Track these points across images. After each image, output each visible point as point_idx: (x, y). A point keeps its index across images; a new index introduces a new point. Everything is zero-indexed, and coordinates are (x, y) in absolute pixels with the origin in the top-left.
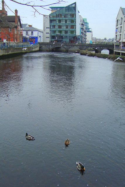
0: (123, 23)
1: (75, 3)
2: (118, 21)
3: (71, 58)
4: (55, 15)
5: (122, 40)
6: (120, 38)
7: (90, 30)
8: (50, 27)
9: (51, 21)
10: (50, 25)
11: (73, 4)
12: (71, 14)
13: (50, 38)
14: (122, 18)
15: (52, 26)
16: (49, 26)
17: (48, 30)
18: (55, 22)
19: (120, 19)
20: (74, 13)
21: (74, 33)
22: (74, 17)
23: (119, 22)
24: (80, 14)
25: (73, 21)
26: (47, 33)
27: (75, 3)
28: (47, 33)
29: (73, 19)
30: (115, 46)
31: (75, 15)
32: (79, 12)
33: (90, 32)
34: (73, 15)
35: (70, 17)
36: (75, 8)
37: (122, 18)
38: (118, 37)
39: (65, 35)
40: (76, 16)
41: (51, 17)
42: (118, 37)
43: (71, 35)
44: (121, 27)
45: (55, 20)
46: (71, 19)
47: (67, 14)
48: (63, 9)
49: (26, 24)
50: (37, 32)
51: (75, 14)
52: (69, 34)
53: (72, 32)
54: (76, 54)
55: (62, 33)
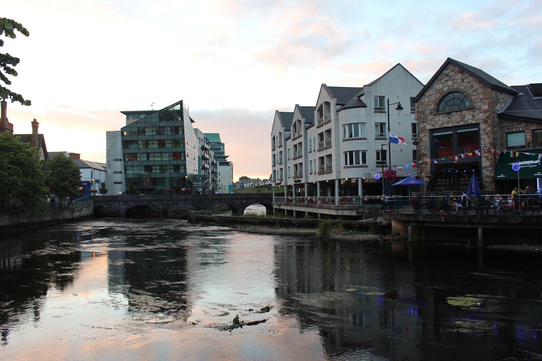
0: (283, 143)
1: (181, 103)
2: (274, 139)
3: (77, 265)
4: (136, 130)
5: (307, 177)
6: (281, 176)
7: (228, 160)
8: (124, 158)
9: (126, 144)
10: (124, 154)
11: (177, 104)
12: (171, 127)
13: (124, 183)
14: (280, 133)
15: (127, 156)
16: (120, 156)
17: (119, 166)
18: (134, 146)
19: (277, 135)
20: (180, 124)
21: (182, 171)
22: (180, 133)
23: (277, 143)
24: (194, 126)
25: (180, 142)
26: (115, 173)
27: (181, 103)
28: (115, 173)
29: (177, 137)
30: (274, 197)
31: (180, 129)
32: (192, 121)
33: (228, 164)
34: (179, 129)
35: (169, 133)
36: (180, 113)
37: (280, 133)
38: (278, 176)
39: (161, 176)
40: (183, 130)
41: (125, 133)
42: (278, 176)
43: (175, 175)
44: (281, 152)
45: (136, 142)
46: (173, 137)
47: (164, 127)
48: (153, 115)
49: (66, 152)
50: (90, 170)
51: (183, 127)
52: (169, 173)
53: (177, 168)
54: (99, 252)
55: (154, 171)
